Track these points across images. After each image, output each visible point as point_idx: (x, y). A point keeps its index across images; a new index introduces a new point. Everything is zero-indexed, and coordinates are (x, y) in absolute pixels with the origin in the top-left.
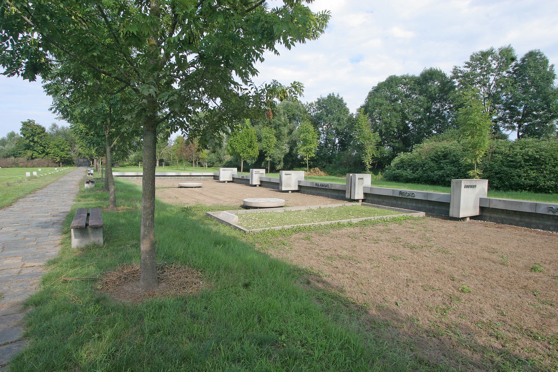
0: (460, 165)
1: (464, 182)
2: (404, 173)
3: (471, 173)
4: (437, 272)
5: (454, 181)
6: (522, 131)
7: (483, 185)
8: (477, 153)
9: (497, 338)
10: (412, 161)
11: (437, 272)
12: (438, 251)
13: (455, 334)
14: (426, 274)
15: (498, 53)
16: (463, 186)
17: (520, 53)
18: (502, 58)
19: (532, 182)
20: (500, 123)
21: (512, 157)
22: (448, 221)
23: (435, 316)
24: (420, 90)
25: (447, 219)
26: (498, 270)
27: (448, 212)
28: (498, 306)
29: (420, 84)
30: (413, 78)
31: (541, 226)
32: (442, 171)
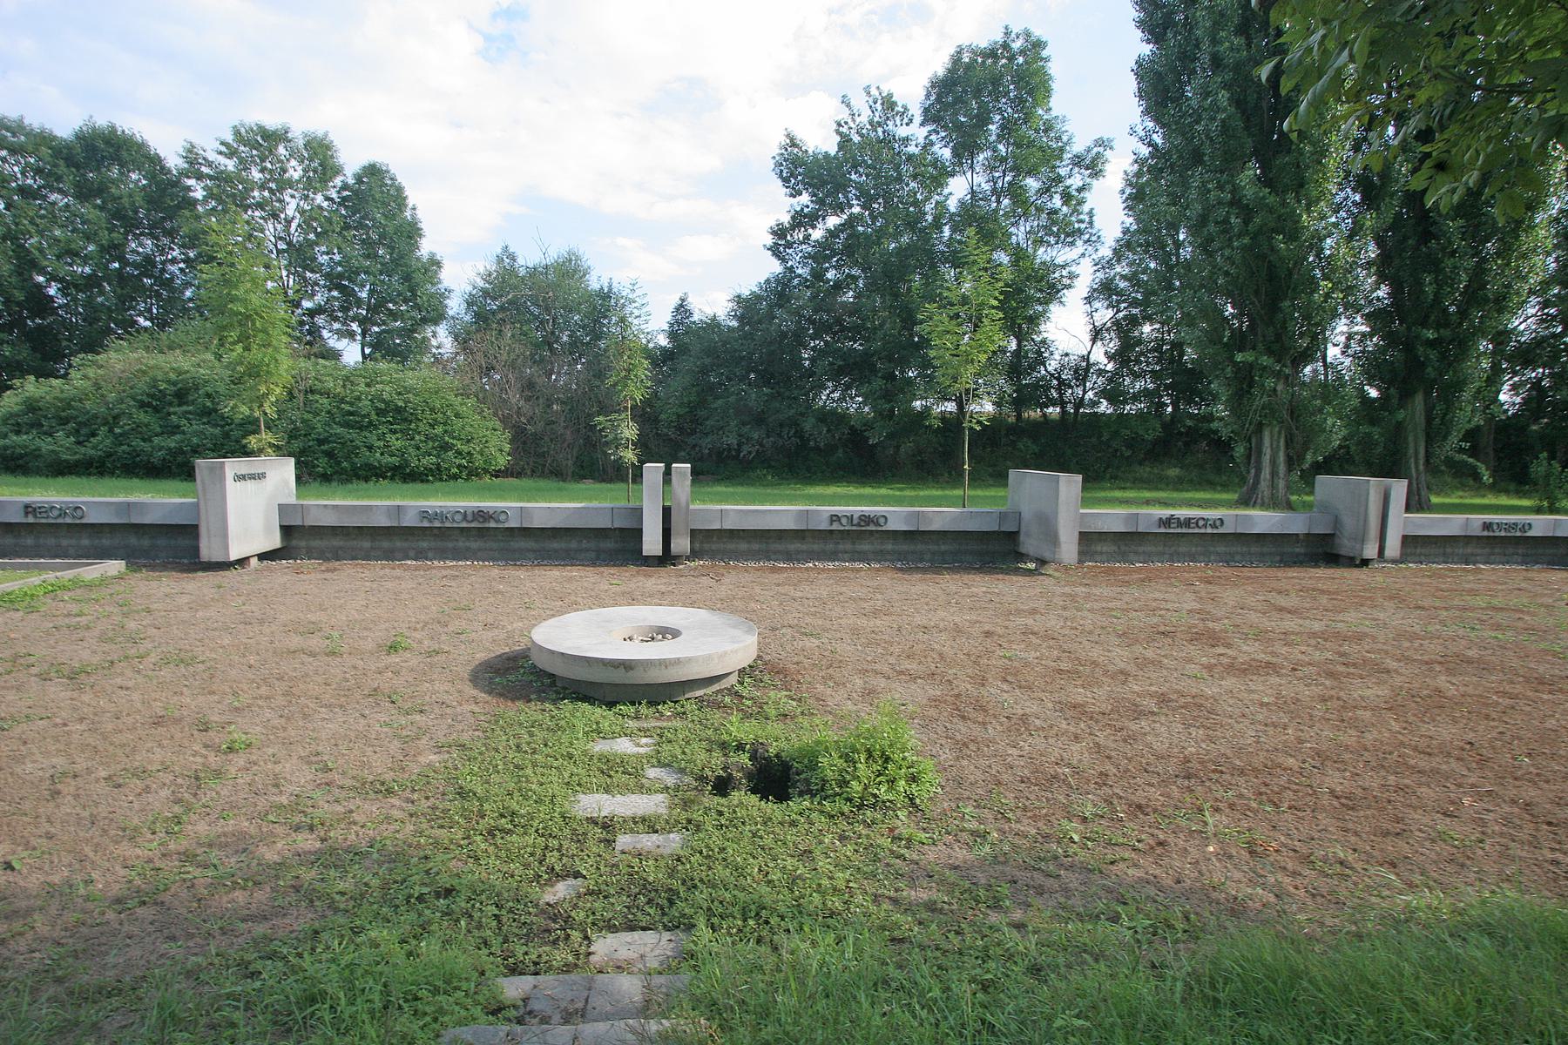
0: (226, 421)
1: (232, 466)
2: (45, 445)
3: (252, 441)
4: (158, 722)
5: (201, 463)
6: (370, 345)
7: (282, 472)
8: (263, 389)
9: (311, 828)
10: (69, 406)
11: (158, 722)
12: (165, 661)
13: (206, 867)
14: (127, 737)
15: (301, 143)
16: (229, 474)
17: (351, 161)
18: (311, 160)
19: (395, 460)
20: (320, 320)
21: (351, 404)
22: (200, 574)
23: (148, 847)
24: (77, 185)
25: (196, 571)
26: (321, 671)
27: (196, 550)
28: (318, 754)
29: (78, 167)
30: (44, 139)
31: (412, 554)
32: (178, 437)
